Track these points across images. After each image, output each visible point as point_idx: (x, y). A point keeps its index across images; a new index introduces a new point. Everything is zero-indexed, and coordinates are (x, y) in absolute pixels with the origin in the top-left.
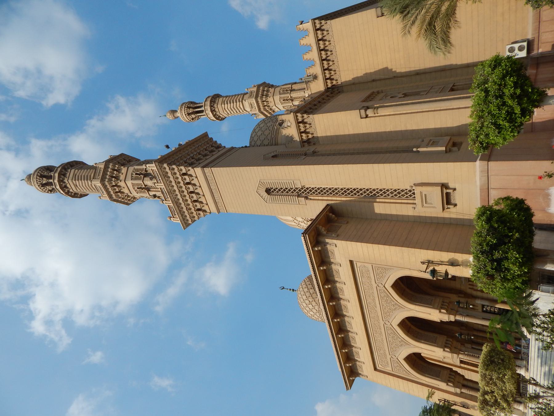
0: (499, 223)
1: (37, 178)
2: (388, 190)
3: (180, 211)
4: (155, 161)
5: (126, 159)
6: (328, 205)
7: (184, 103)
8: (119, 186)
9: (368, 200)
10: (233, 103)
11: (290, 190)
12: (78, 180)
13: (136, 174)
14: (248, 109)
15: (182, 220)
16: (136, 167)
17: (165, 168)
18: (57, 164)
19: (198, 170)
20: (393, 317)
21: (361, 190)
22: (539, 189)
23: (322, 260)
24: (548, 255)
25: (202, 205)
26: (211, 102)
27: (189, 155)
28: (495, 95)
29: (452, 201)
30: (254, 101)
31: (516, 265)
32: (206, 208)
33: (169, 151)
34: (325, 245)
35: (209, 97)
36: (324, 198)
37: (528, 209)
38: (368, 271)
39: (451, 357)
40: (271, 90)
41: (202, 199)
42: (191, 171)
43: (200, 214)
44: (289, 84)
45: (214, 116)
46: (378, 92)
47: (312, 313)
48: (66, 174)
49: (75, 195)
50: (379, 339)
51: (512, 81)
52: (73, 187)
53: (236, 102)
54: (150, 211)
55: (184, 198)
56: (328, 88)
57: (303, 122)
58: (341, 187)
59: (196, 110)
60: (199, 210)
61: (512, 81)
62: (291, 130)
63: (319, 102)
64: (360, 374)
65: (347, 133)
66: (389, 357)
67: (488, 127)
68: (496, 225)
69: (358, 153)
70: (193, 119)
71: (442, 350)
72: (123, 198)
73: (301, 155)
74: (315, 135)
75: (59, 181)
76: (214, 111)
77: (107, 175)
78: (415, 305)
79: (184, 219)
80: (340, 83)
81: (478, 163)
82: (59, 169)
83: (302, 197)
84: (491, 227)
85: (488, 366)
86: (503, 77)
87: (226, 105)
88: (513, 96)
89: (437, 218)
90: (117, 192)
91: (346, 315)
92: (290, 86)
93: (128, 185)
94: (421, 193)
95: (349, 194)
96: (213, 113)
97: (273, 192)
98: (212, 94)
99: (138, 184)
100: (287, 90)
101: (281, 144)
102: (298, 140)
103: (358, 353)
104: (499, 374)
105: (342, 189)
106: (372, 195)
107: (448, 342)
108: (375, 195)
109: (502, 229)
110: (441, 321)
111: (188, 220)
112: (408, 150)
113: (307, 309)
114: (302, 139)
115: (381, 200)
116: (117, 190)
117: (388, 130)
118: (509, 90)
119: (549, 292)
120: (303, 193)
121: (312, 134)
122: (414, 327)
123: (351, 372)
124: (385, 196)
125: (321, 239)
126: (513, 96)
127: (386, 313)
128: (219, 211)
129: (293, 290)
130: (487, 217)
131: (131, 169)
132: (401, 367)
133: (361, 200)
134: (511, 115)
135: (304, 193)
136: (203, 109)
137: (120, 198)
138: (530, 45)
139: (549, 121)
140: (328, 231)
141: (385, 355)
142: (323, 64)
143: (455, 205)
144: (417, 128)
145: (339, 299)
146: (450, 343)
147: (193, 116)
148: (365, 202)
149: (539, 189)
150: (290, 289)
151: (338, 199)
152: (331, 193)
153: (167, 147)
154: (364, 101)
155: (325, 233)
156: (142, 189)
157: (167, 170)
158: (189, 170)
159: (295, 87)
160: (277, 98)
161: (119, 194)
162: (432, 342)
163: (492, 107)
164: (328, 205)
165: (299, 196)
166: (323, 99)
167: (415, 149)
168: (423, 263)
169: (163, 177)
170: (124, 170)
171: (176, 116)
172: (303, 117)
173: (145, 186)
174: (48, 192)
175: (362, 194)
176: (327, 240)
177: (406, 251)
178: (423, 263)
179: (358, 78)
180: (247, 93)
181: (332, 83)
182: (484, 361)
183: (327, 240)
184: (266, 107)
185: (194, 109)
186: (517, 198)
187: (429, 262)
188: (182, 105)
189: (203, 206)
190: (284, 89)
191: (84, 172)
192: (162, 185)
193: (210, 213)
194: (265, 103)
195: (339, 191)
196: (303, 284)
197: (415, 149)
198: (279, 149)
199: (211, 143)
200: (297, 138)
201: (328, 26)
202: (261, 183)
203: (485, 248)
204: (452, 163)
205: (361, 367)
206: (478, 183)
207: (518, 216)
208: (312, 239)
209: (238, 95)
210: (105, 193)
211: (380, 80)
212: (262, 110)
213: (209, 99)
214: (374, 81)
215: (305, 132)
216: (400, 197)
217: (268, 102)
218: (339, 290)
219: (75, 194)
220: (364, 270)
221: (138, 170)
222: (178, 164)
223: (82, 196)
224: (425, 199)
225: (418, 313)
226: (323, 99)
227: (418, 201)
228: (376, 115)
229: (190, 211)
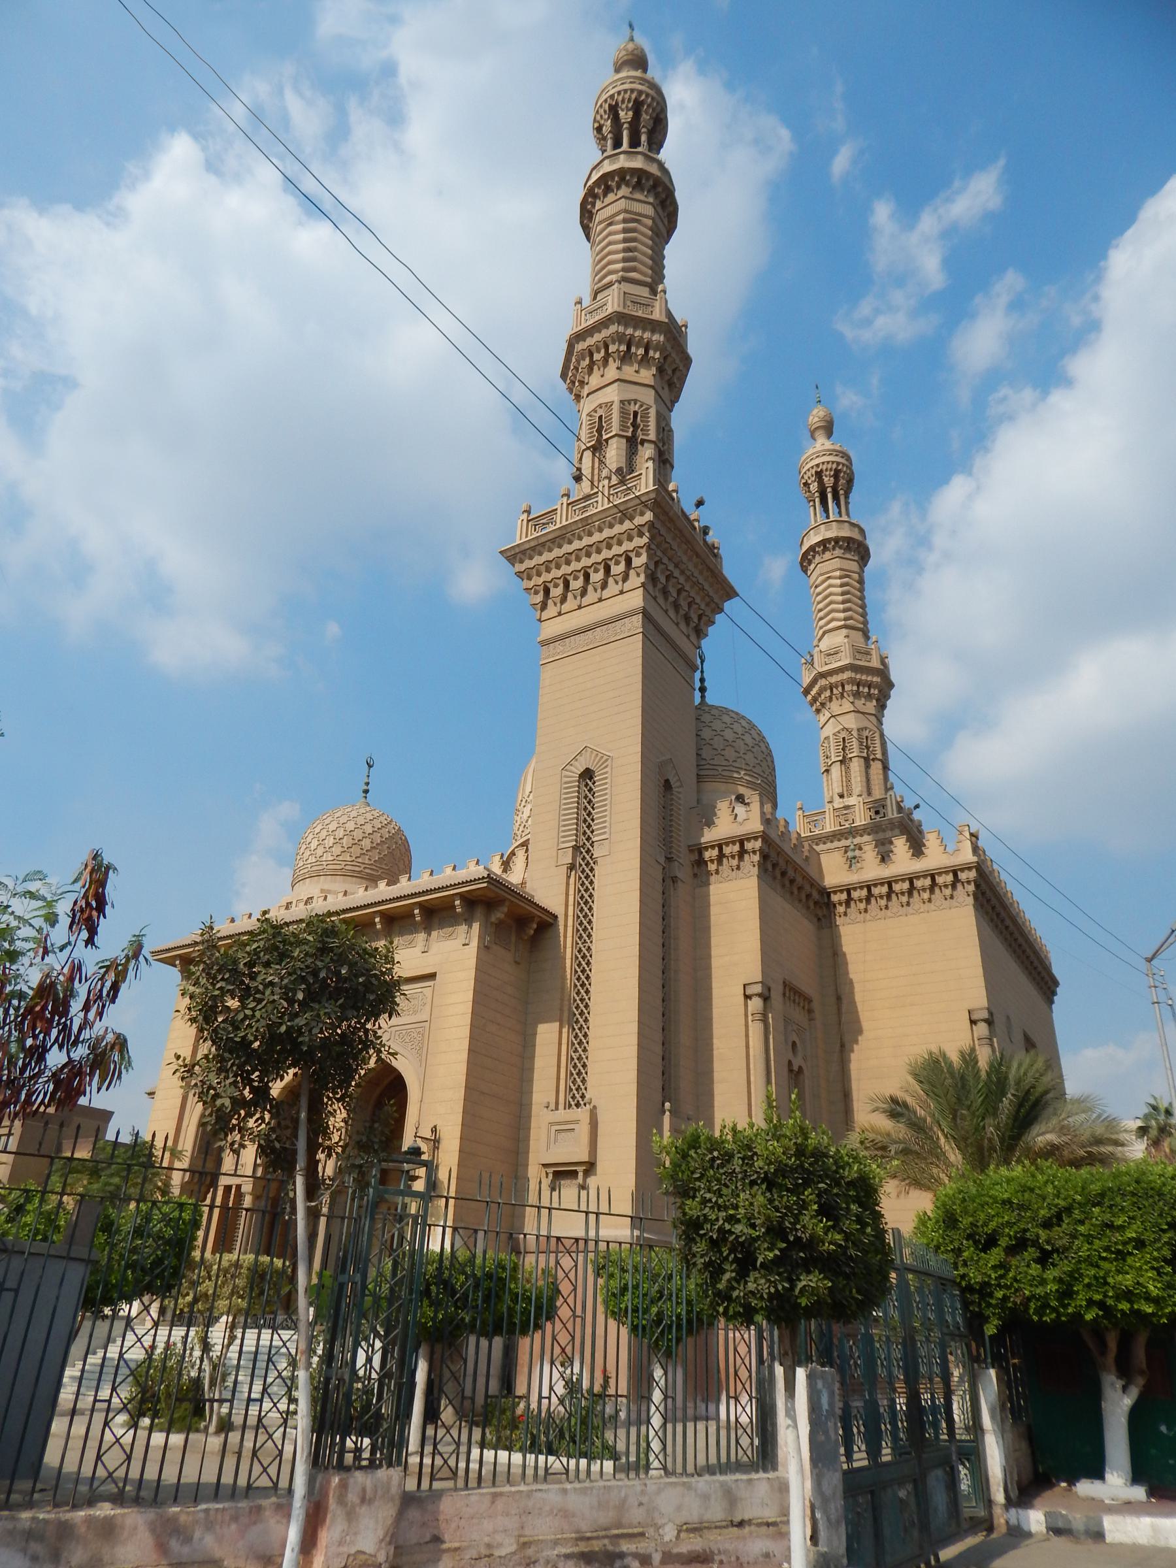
1: (632, 91)
2: (585, 1050)
5: (678, 374)
6: (556, 917)
7: (849, 459)
9: (566, 1008)
12: (625, 231)
13: (636, 414)
14: (825, 644)
15: (523, 548)
16: (652, 412)
17: (642, 514)
19: (635, 599)
21: (587, 992)
26: (849, 540)
32: (551, 610)
36: (571, 909)
38: (415, 1012)
40: (871, 707)
42: (636, 580)
43: (536, 593)
45: (812, 548)
46: (810, 1011)
47: (313, 846)
48: (642, 190)
49: (586, 214)
53: (844, 611)
55: (573, 556)
56: (829, 894)
57: (742, 853)
60: (547, 591)
74: (713, 878)
76: (825, 549)
77: (635, 328)
79: (523, 552)
80: (839, 921)
82: (653, 169)
83: (574, 858)
87: (838, 582)
89: (528, 1152)
92: (879, 756)
93: (609, 390)
94: (577, 1122)
96: (818, 544)
97: (587, 785)
98: (871, 544)
101: (699, 791)
104: (243, 1289)
105: (589, 949)
106: (575, 1018)
108: (577, 1022)
112: (667, 1091)
113: (324, 833)
114: (706, 848)
115: (565, 1035)
120: (584, 859)
121: (717, 872)
124: (573, 1044)
125: (479, 912)
128: (545, 643)
129: (366, 792)
131: (648, 397)
135: (582, 862)
137: (578, 362)
142: (882, 884)
144: (716, 1104)
147: (814, 487)
150: (367, 784)
151: (569, 940)
155: (493, 919)
156: (599, 431)
157: (639, 520)
158: (638, 575)
159: (876, 767)
160: (851, 722)
165: (576, 848)
168: (434, 1130)
170: (647, 375)
171: (817, 434)
173: (607, 440)
174: (595, 120)
175: (578, 993)
176: (476, 926)
177: (457, 1095)
178: (434, 1130)
181: (840, 904)
183: (476, 926)
187: (436, 1142)
188: (845, 455)
191: (644, 249)
195: (585, 942)
196: (382, 819)
197: (667, 1105)
198: (685, 794)
200: (709, 836)
201: (961, 900)
202: (605, 760)
208: (479, 893)
209: (864, 615)
212: (822, 682)
213: (856, 535)
214: (839, 999)
215: (721, 856)
216: (572, 1074)
217: (842, 696)
221: (646, 416)
224: (564, 1128)
226: (800, 889)
227: (562, 1114)
228: (750, 1018)
229: (543, 568)
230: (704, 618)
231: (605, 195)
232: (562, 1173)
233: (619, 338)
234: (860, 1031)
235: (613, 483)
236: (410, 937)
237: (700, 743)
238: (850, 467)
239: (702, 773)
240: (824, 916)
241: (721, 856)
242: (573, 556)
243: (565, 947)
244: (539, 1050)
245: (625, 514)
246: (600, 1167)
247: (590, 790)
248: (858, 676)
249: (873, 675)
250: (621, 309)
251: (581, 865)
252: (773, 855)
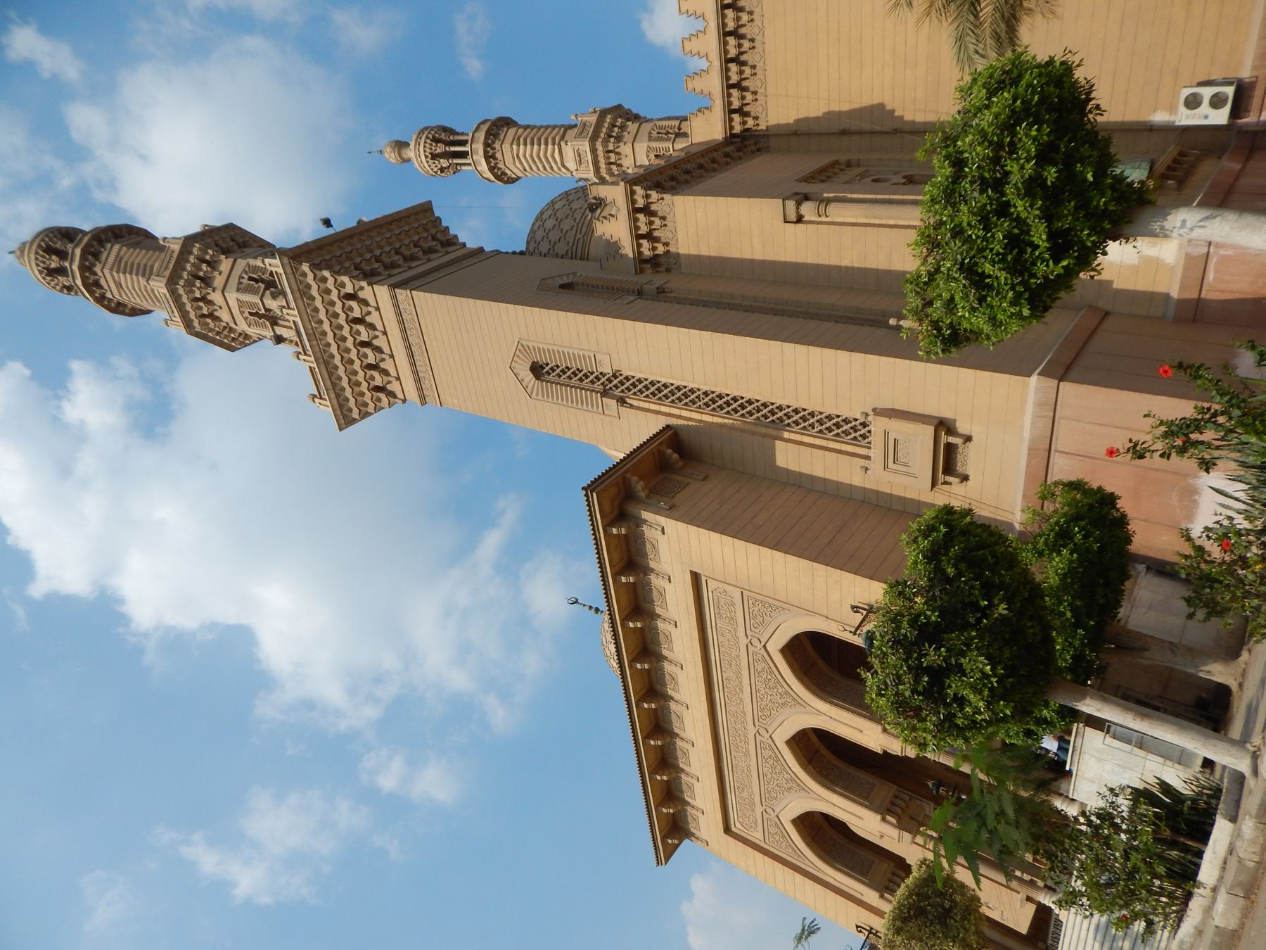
0: (963, 566)
1: (37, 253)
3: (334, 385)
4: (282, 253)
6: (668, 426)
7: (426, 128)
8: (210, 303)
9: (763, 430)
10: (539, 144)
11: (587, 377)
13: (251, 279)
14: (571, 165)
15: (337, 407)
17: (305, 275)
18: (87, 227)
19: (382, 292)
20: (778, 722)
22: (1174, 473)
23: (627, 564)
24: (1145, 650)
25: (386, 379)
27: (371, 251)
28: (982, 178)
29: (960, 468)
30: (585, 147)
31: (981, 693)
32: (394, 387)
33: (330, 231)
34: (638, 526)
35: (484, 122)
37: (1122, 521)
38: (733, 604)
39: (896, 837)
40: (632, 127)
41: (387, 365)
43: (379, 400)
44: (677, 118)
45: (492, 169)
46: (849, 164)
48: (100, 252)
49: (119, 308)
50: (742, 763)
51: (1035, 139)
54: (278, 372)
55: (345, 355)
56: (733, 136)
57: (647, 210)
58: (704, 388)
59: (453, 149)
61: (1035, 139)
62: (615, 229)
63: (701, 166)
64: (693, 835)
65: (747, 255)
66: (759, 809)
67: (949, 278)
68: (951, 571)
69: (749, 309)
70: (442, 170)
71: (879, 817)
72: (218, 333)
73: (629, 292)
74: (672, 249)
75: (82, 268)
76: (493, 156)
78: (832, 703)
79: (341, 406)
80: (762, 127)
81: (1034, 379)
82: (86, 239)
83: (613, 397)
84: (939, 570)
85: (905, 920)
86: (1009, 125)
88: (1033, 187)
90: (204, 316)
91: (672, 698)
92: (677, 123)
93: (230, 303)
94: (886, 434)
95: (721, 408)
98: (493, 117)
99: (251, 305)
100: (668, 133)
102: (631, 255)
103: (691, 788)
105: (706, 394)
106: (777, 419)
107: (898, 802)
108: (781, 419)
109: (965, 583)
110: (885, 752)
111: (351, 410)
112: (877, 321)
114: (640, 253)
116: (205, 311)
117: (844, 263)
118: (1022, 168)
119: (1129, 742)
121: (666, 244)
122: (822, 754)
123: (672, 828)
125: (631, 508)
126: (1033, 187)
127: (762, 710)
130: (933, 543)
131: (241, 264)
132: (784, 837)
133: (747, 427)
134: (1022, 251)
135: (617, 388)
136: (467, 148)
137: (211, 330)
138: (1243, 92)
139: (1243, 301)
140: (654, 491)
141: (752, 805)
142: (728, 70)
143: (965, 478)
145: (660, 658)
146: (903, 805)
147: (444, 163)
148: (754, 433)
149: (1174, 473)
152: (680, 399)
153: (327, 223)
154: (800, 180)
158: (362, 288)
161: (209, 320)
162: (860, 796)
163: (964, 217)
165: (605, 394)
166: (713, 161)
167: (892, 322)
168: (855, 609)
169: (298, 295)
170: (225, 264)
171: (404, 156)
172: (648, 196)
174: (61, 291)
175: (751, 414)
176: (646, 515)
178: (855, 609)
179: (807, 119)
180: (576, 126)
181: (744, 123)
182: (900, 907)
183: (646, 515)
185: (447, 145)
186: (1100, 488)
188: (422, 132)
189: (389, 382)
190: (661, 128)
192: (293, 315)
193: (404, 401)
194: (612, 155)
195: (698, 397)
197: (892, 322)
198: (584, 271)
199: (433, 231)
200: (628, 250)
202: (522, 348)
203: (905, 629)
204: (972, 371)
205: (696, 820)
206: (1027, 433)
207: (1085, 537)
209: (554, 127)
210: (176, 314)
211: (861, 133)
213: (485, 127)
214: (844, 132)
216: (838, 435)
217: (619, 154)
218: (662, 637)
219: (119, 304)
220: (722, 601)
222: (337, 268)
223: (135, 312)
224: (893, 451)
225: (834, 723)
226: (713, 161)
227: (876, 452)
228: (823, 219)
230: (439, 236)
231: (102, 287)
232: (947, 463)
233: (189, 285)
234: (881, 106)
235: (284, 304)
236: (655, 593)
237: (551, 253)
238: (432, 128)
240: (755, 144)
241: (649, 236)
242: (345, 355)
243: (701, 421)
244: (805, 469)
245: (303, 292)
246: (946, 414)
247: (552, 369)
248: (602, 135)
249: (604, 121)
250: (165, 280)
252: (659, 178)
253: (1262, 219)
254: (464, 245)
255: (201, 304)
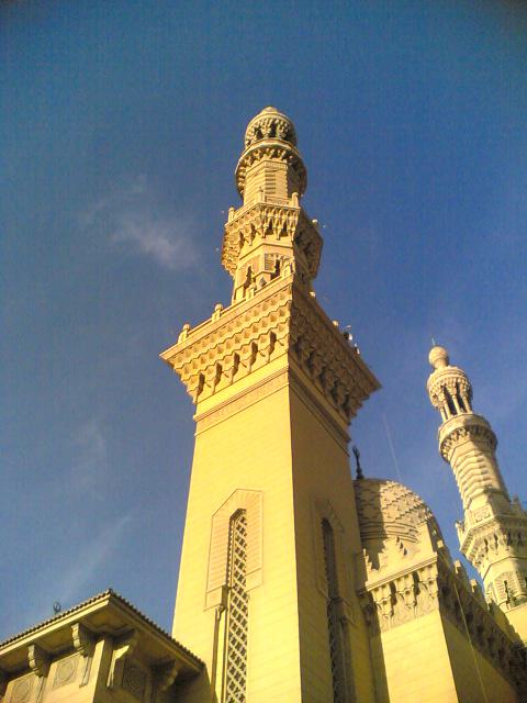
8: (253, 237)
35: (487, 423)
42: (282, 349)
52: (254, 171)
98: (494, 427)
99: (256, 265)
131: (290, 254)
135: (232, 601)
164: (202, 665)
165: (226, 589)
166: (491, 640)
184: (484, 546)
194: (493, 541)
195: (238, 690)
208: (101, 619)
239: (365, 531)
251: (232, 607)
253: (306, 694)
254: (349, 424)
255: (251, 231)
